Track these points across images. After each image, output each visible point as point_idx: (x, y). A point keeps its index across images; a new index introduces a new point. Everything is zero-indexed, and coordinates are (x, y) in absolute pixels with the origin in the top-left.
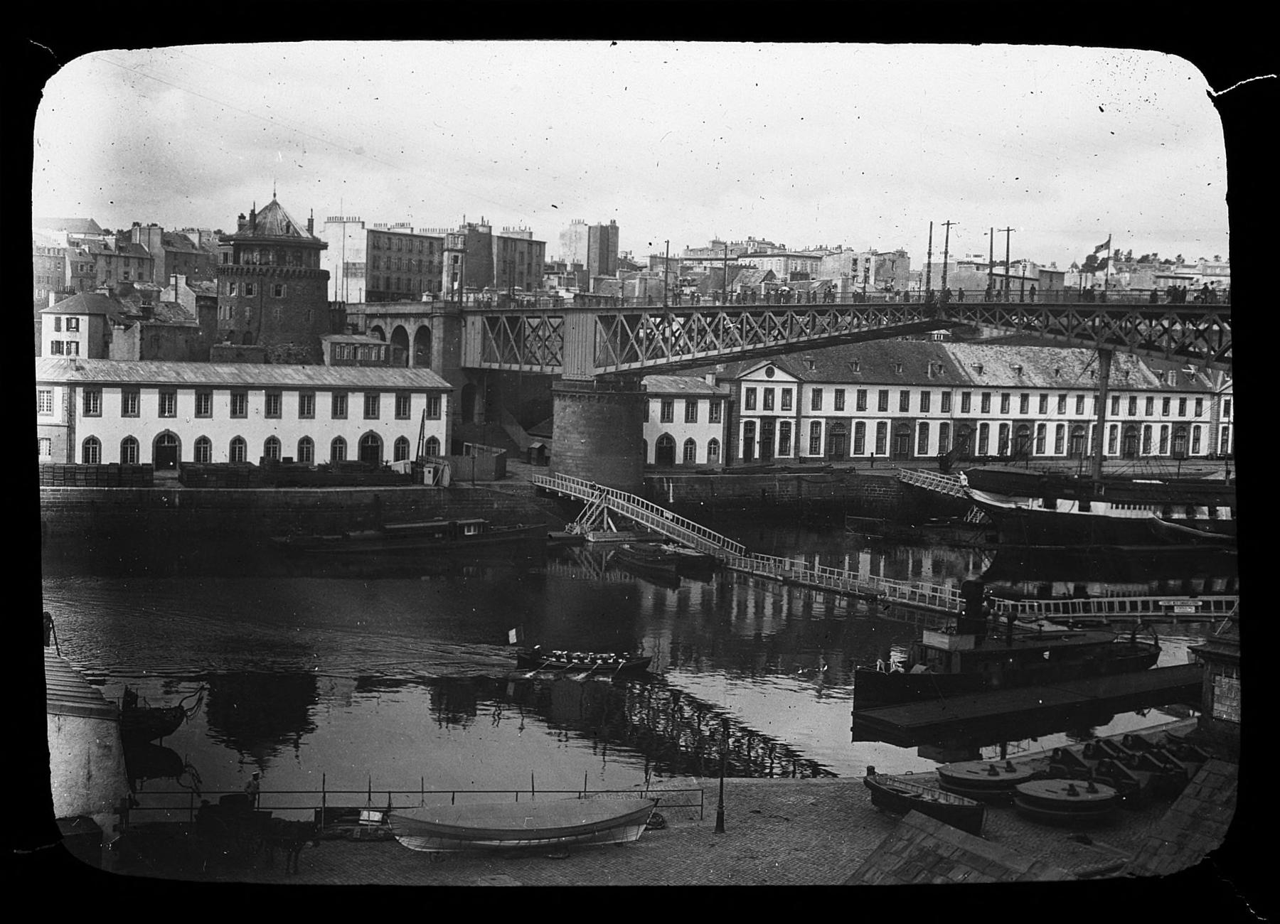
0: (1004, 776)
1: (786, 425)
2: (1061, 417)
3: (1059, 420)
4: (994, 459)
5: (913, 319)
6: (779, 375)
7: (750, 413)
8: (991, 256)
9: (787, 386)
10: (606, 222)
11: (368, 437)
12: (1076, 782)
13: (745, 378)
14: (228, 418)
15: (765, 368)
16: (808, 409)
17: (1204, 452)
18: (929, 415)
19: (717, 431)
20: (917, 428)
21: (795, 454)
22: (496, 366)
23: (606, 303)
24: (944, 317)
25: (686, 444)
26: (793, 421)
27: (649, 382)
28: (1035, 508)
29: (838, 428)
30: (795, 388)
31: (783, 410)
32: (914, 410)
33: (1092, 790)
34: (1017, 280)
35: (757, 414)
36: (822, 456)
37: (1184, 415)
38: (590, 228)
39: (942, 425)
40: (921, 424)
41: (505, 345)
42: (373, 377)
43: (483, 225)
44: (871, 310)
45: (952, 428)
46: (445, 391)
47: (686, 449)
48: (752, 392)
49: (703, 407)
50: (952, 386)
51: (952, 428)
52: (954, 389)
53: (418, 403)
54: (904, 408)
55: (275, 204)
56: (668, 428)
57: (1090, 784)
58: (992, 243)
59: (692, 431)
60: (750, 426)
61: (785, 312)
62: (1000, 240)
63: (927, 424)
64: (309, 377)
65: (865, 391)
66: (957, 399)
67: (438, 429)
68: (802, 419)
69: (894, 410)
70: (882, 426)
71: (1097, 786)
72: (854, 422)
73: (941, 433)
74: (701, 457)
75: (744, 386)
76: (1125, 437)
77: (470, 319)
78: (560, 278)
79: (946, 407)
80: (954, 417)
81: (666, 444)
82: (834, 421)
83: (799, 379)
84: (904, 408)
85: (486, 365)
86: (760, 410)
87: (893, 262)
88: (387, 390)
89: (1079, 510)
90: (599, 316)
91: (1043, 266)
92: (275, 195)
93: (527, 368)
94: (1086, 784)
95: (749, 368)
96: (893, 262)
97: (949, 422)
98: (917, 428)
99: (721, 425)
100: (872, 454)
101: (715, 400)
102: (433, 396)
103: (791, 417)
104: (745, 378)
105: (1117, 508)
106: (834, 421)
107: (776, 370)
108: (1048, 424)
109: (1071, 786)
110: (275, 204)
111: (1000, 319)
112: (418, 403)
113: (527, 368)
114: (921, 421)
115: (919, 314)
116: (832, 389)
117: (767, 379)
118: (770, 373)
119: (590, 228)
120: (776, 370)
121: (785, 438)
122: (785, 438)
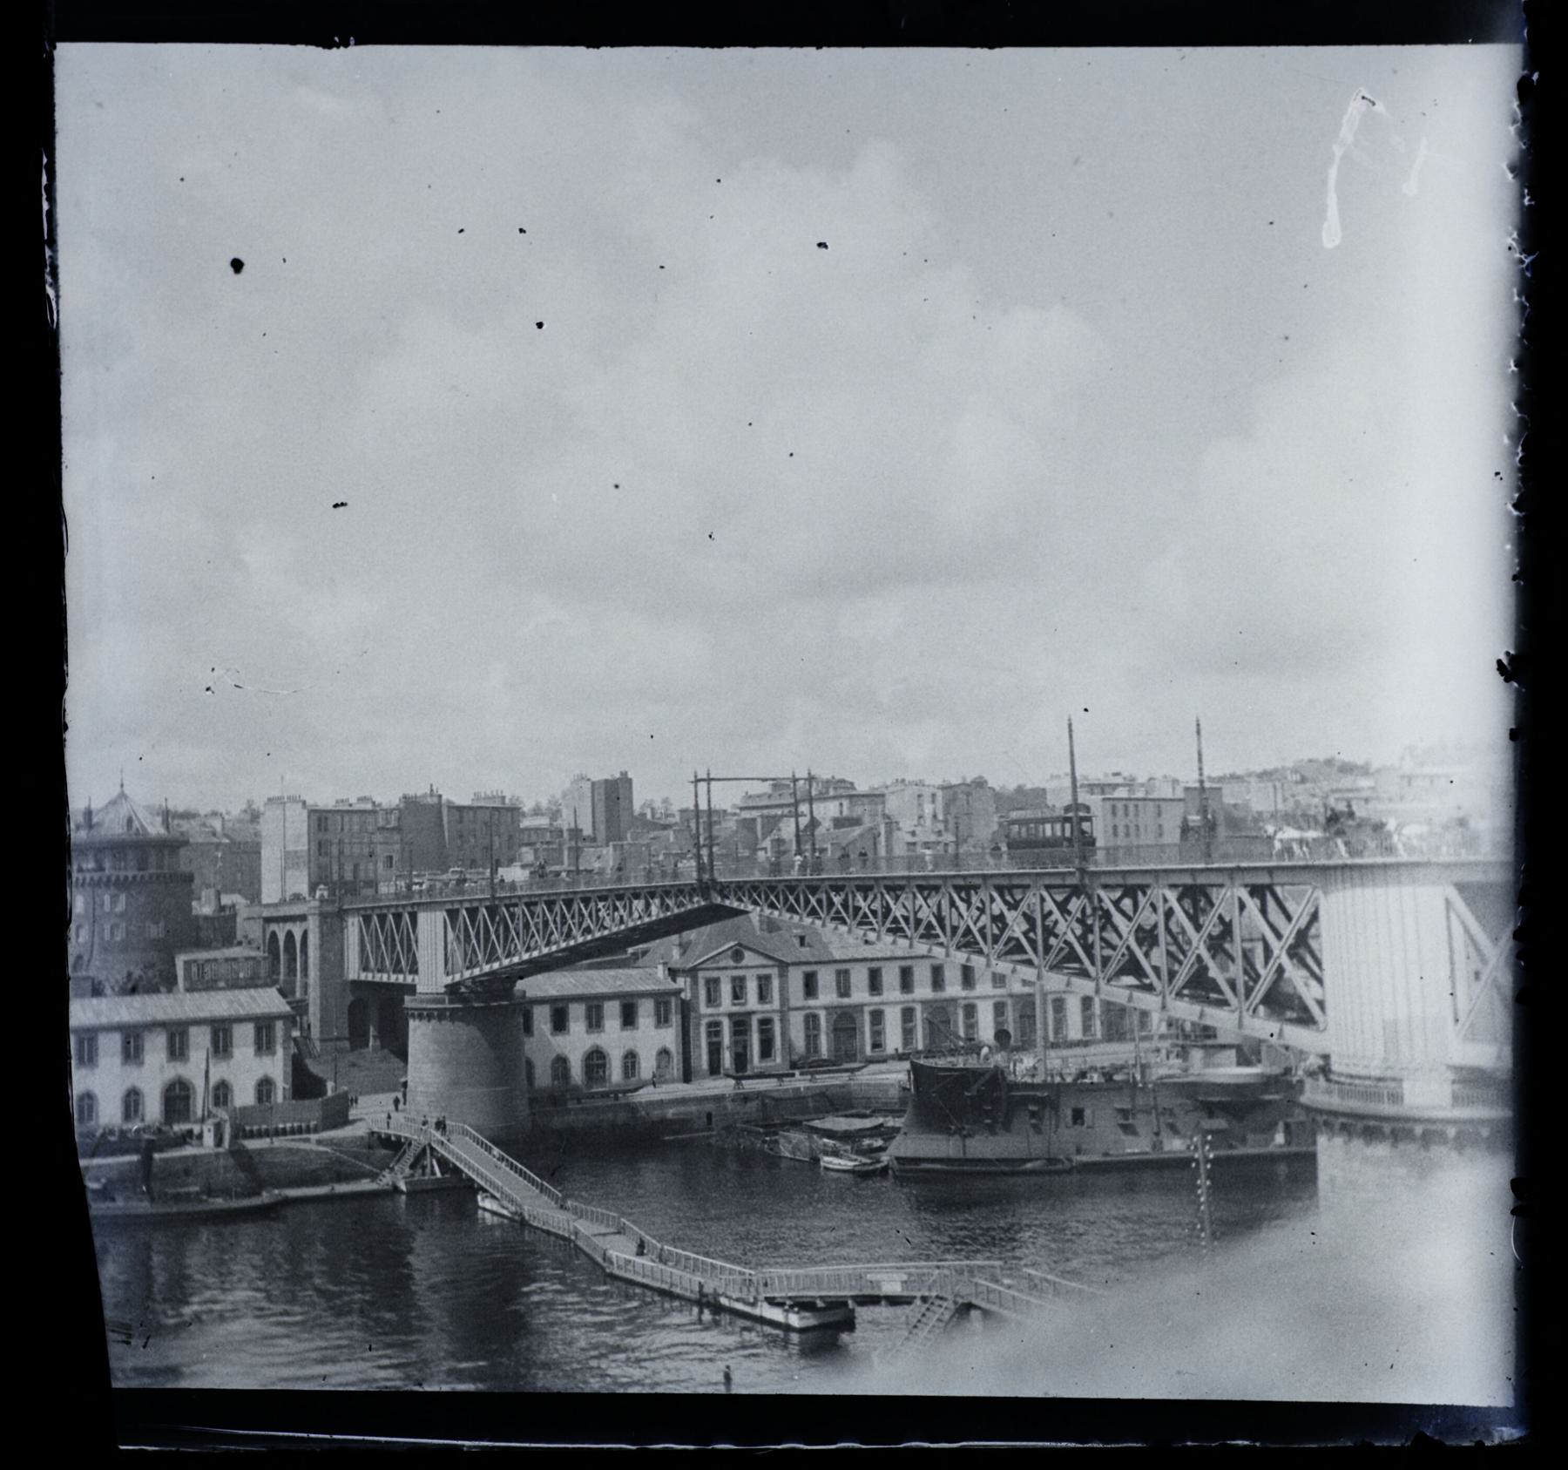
1: (765, 1023)
3: (904, 1002)
8: (709, 801)
10: (612, 772)
11: (592, 1053)
15: (729, 953)
19: (669, 1037)
23: (421, 897)
25: (626, 1057)
26: (776, 1018)
27: (534, 986)
30: (774, 972)
34: (1151, 804)
37: (880, 994)
38: (593, 784)
39: (807, 1018)
41: (393, 952)
42: (219, 1004)
43: (432, 795)
49: (646, 1009)
55: (123, 796)
65: (847, 972)
72: (867, 1009)
73: (807, 1028)
78: (536, 851)
85: (363, 976)
86: (726, 1003)
87: (968, 794)
91: (1187, 782)
92: (122, 785)
96: (968, 794)
103: (774, 1011)
106: (839, 1012)
107: (747, 954)
108: (193, 1030)
110: (123, 796)
117: (735, 965)
119: (593, 784)
120: (747, 954)
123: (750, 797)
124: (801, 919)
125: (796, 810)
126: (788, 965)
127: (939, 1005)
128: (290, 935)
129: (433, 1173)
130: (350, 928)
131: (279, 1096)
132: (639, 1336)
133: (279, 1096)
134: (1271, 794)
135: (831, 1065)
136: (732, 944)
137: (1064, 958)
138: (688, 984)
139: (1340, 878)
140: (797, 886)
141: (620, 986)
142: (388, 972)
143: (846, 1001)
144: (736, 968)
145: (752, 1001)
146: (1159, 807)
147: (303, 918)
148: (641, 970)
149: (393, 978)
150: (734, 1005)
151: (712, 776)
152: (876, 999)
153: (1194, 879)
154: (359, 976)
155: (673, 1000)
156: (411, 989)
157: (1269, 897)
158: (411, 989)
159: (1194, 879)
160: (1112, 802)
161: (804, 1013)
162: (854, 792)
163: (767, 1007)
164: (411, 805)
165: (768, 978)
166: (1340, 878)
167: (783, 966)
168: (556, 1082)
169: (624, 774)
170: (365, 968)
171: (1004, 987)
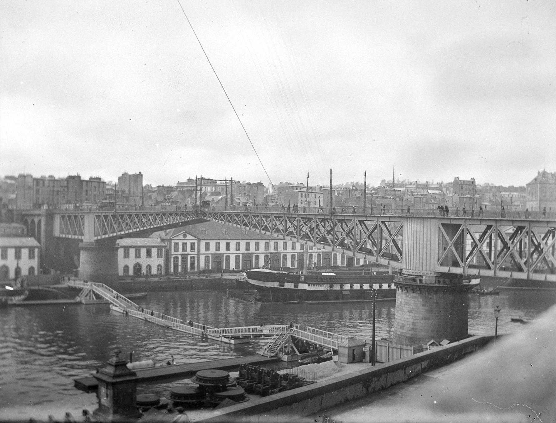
2: (268, 251)
3: (318, 252)
4: (233, 271)
6: (189, 237)
11: (136, 265)
13: (173, 239)
15: (182, 234)
19: (161, 261)
21: (197, 269)
25: (147, 267)
27: (119, 241)
28: (276, 287)
30: (196, 242)
31: (191, 251)
35: (241, 252)
36: (241, 269)
37: (229, 250)
39: (236, 256)
40: (256, 256)
45: (322, 256)
46: (37, 247)
49: (154, 251)
50: (269, 240)
51: (322, 256)
52: (270, 241)
53: (25, 252)
54: (248, 249)
56: (138, 260)
59: (149, 261)
60: (176, 259)
63: (312, 254)
66: (272, 244)
67: (35, 263)
68: (201, 255)
69: (243, 249)
70: (293, 256)
75: (173, 242)
80: (271, 252)
83: (199, 239)
84: (248, 249)
85: (61, 236)
86: (180, 251)
89: (294, 287)
90: (442, 224)
95: (178, 233)
97: (268, 254)
99: (163, 258)
100: (233, 269)
101: (159, 248)
102: (31, 250)
104: (173, 239)
105: (316, 286)
107: (187, 235)
114: (175, 256)
117: (183, 238)
118: (185, 236)
120: (187, 235)
123: (180, 183)
124: (232, 225)
125: (196, 188)
126: (201, 239)
127: (247, 255)
128: (33, 221)
129: (93, 299)
130: (56, 220)
131: (36, 273)
132: (164, 353)
134: (348, 194)
135: (212, 272)
136: (183, 232)
138: (168, 244)
139: (410, 221)
140: (239, 215)
141: (146, 243)
142: (71, 235)
144: (184, 240)
146: (315, 195)
147: (39, 215)
148: (152, 239)
149: (73, 237)
150: (191, 251)
152: (228, 252)
153: (344, 218)
154: (59, 235)
155: (163, 249)
158: (82, 240)
159: (344, 218)
160: (301, 193)
161: (264, 255)
162: (216, 184)
163: (176, 253)
165: (194, 243)
166: (410, 221)
167: (199, 240)
168: (125, 274)
169: (140, 173)
170: (62, 233)
171: (268, 250)
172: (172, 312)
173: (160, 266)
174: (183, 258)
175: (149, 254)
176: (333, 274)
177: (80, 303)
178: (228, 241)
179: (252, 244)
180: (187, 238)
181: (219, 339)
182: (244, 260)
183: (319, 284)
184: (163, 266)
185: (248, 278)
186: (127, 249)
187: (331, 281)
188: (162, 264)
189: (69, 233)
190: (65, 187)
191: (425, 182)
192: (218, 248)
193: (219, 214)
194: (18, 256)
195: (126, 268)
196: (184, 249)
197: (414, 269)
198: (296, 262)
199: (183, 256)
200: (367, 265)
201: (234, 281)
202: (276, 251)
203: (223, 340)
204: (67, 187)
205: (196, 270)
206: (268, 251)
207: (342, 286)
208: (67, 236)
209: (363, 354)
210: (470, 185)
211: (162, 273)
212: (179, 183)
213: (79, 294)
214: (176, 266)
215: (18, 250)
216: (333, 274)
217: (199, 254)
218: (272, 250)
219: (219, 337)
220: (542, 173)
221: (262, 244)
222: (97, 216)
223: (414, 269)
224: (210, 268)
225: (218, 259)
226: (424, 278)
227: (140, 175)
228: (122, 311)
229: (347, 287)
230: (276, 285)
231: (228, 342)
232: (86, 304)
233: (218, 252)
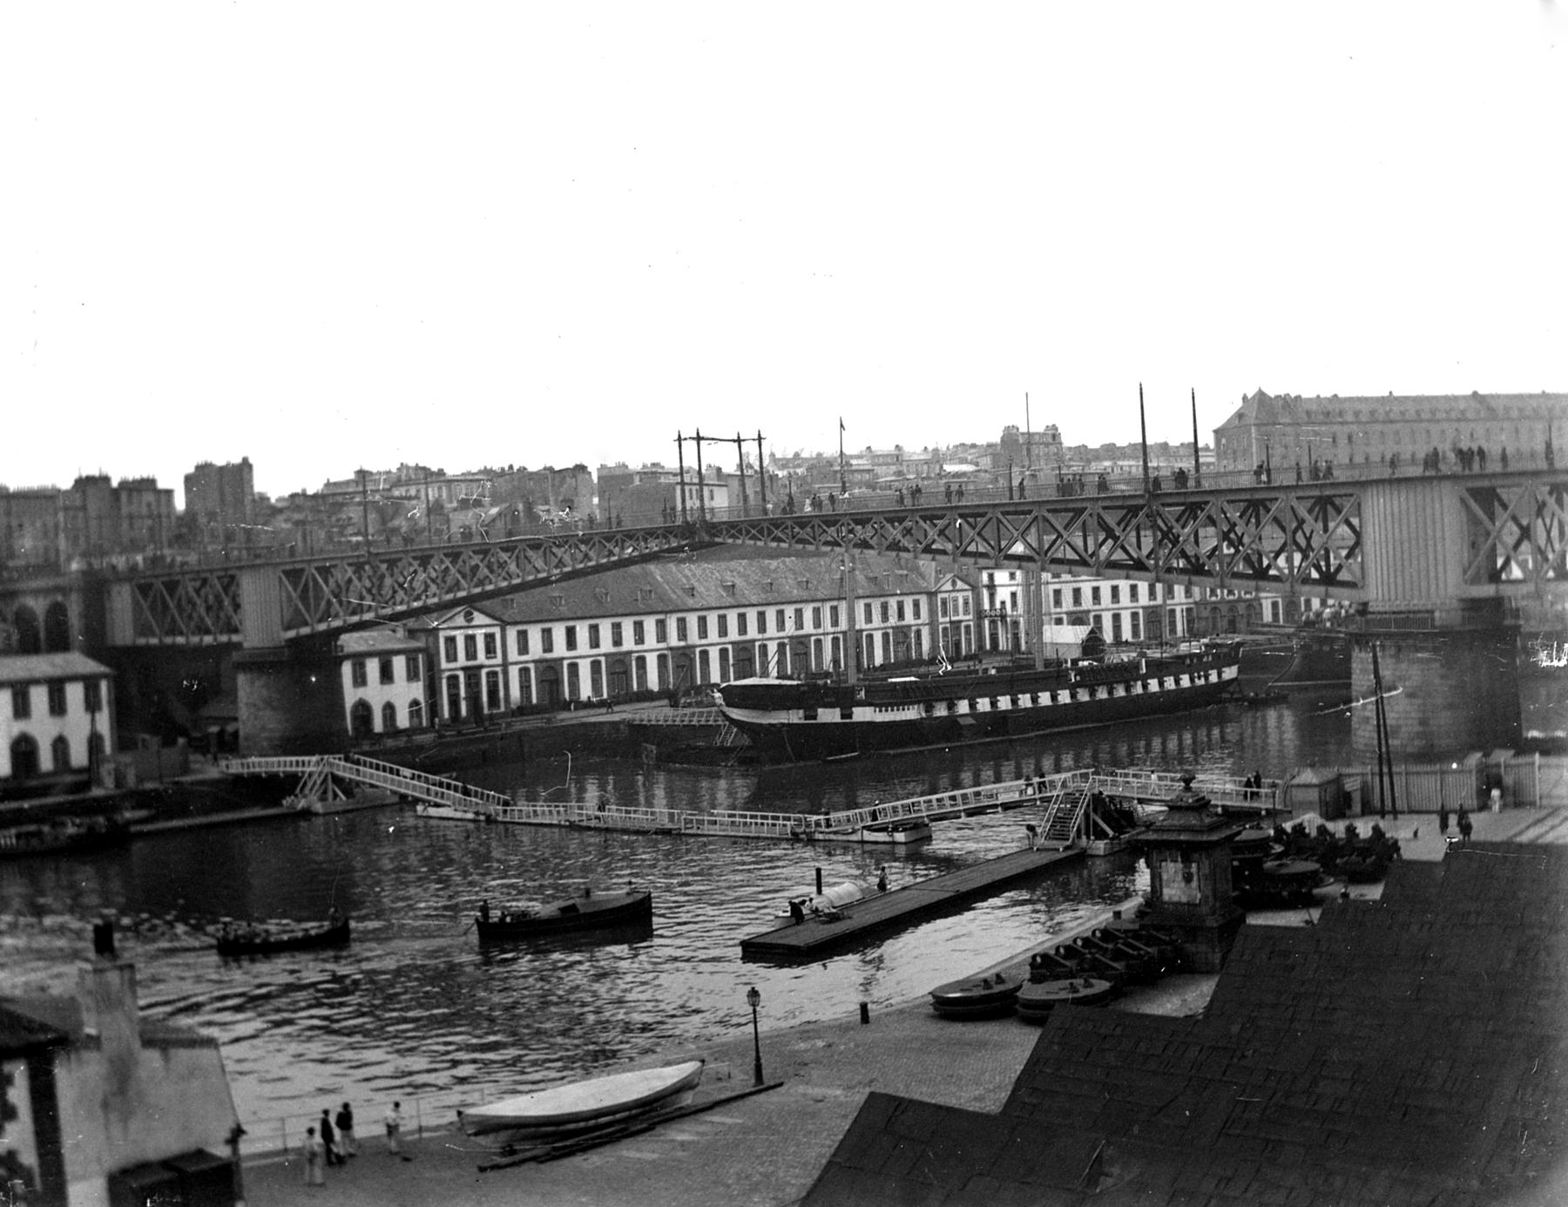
0: (998, 989)
2: (782, 634)
4: (589, 705)
5: (669, 542)
6: (479, 618)
7: (452, 665)
9: (489, 630)
12: (1074, 981)
14: (379, 686)
16: (513, 655)
17: (879, 660)
18: (1120, 605)
19: (418, 691)
20: (634, 663)
22: (154, 641)
24: (707, 538)
29: (550, 671)
30: (497, 631)
31: (487, 658)
32: (629, 643)
33: (1088, 985)
40: (449, 678)
44: (596, 539)
46: (105, 676)
47: (384, 716)
48: (451, 641)
49: (399, 664)
50: (666, 613)
53: (75, 694)
54: (617, 641)
56: (361, 693)
57: (1086, 981)
58: (1195, 431)
60: (453, 680)
61: (516, 547)
62: (750, 448)
64: (54, 666)
69: (606, 645)
70: (595, 666)
71: (1093, 981)
72: (566, 663)
74: (403, 721)
75: (442, 635)
76: (795, 654)
77: (115, 589)
79: (662, 636)
81: (363, 709)
82: (545, 664)
84: (617, 641)
85: (142, 641)
86: (462, 660)
88: (37, 682)
93: (195, 639)
94: (1082, 981)
98: (444, 682)
102: (90, 683)
106: (545, 664)
107: (476, 614)
108: (1103, 614)
109: (1071, 984)
111: (769, 535)
112: (75, 694)
113: (195, 639)
115: (675, 536)
116: (586, 624)
118: (954, 583)
121: (493, 693)
122: (493, 693)
131: (108, 747)
133: (108, 747)
137: (1485, 513)
143: (1095, 584)
145: (481, 657)
151: (683, 443)
152: (572, 653)
156: (238, 646)
157: (1329, 507)
161: (1129, 611)
164: (85, 484)
169: (245, 460)
172: (642, 799)
173: (415, 703)
174: (468, 678)
175: (386, 675)
176: (913, 679)
177: (307, 814)
178: (571, 623)
179: (559, 633)
180: (474, 623)
181: (854, 838)
182: (1148, 622)
183: (898, 705)
184: (423, 705)
185: (728, 705)
186: (359, 660)
187: (924, 694)
188: (421, 698)
189: (174, 631)
190: (77, 509)
191: (892, 448)
192: (548, 646)
193: (765, 525)
194: (58, 707)
195: (388, 712)
196: (471, 654)
197: (1393, 598)
198: (731, 669)
199: (469, 672)
200: (890, 664)
201: (622, 726)
202: (682, 644)
203: (866, 839)
204: (84, 508)
205: (502, 709)
206: (1191, 600)
207: (951, 707)
208: (168, 640)
209: (1347, 797)
210: (1047, 445)
211: (421, 723)
212: (328, 484)
213: (295, 788)
214: (454, 703)
215: (56, 688)
216: (913, 679)
217: (505, 665)
218: (673, 640)
219: (854, 832)
220: (1254, 397)
221: (650, 624)
222: (286, 573)
223: (1393, 598)
224: (534, 701)
225: (550, 671)
226: (1437, 614)
227: (246, 466)
228: (470, 816)
229: (963, 707)
230: (795, 717)
231: (888, 839)
232: (325, 815)
233: (548, 656)
